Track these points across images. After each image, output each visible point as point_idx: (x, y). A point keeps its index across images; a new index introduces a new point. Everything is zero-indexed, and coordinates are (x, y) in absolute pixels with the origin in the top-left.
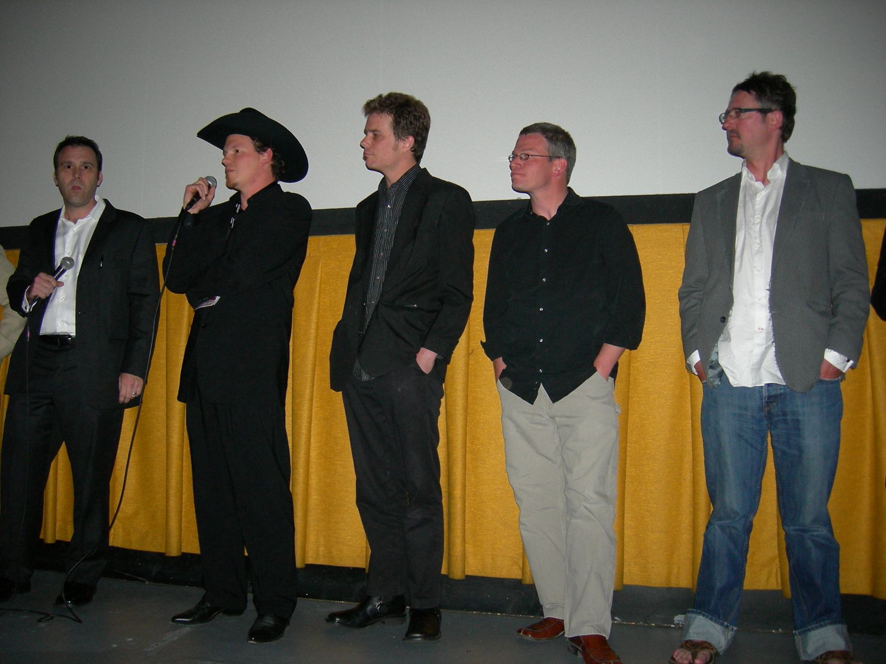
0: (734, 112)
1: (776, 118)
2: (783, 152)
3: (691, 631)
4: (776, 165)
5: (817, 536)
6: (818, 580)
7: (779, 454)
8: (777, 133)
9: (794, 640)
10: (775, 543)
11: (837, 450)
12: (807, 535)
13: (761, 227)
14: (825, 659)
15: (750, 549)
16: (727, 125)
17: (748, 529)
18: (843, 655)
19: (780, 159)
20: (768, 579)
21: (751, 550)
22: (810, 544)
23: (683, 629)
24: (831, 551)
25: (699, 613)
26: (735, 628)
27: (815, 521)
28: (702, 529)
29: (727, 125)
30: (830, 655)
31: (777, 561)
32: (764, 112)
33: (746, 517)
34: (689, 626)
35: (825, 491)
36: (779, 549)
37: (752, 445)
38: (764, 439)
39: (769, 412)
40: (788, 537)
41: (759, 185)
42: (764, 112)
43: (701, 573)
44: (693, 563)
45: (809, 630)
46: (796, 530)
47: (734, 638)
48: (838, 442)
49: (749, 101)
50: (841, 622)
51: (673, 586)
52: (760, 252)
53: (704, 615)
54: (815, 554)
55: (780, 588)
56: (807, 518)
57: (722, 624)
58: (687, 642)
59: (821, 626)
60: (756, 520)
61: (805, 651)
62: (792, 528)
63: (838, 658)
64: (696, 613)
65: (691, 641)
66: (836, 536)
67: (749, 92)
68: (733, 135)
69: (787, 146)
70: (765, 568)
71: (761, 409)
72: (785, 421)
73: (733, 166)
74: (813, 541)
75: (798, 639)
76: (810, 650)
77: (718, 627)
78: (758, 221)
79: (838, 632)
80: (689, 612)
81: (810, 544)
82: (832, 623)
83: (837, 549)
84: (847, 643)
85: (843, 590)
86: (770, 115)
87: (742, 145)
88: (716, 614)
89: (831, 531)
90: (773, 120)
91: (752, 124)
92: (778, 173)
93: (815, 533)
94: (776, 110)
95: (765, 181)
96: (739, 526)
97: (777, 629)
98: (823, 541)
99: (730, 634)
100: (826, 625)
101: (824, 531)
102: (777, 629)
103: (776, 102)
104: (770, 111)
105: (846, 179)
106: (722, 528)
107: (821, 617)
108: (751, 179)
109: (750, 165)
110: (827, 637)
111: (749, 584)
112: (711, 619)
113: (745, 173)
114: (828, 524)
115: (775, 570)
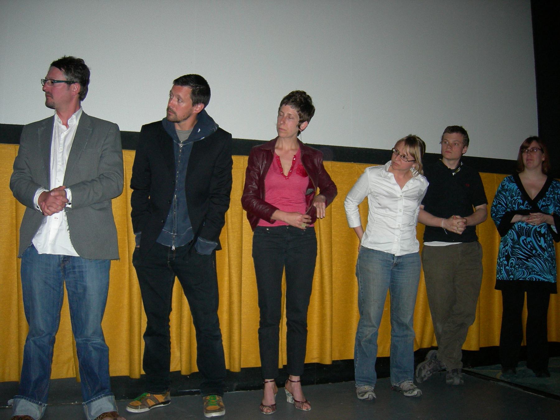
0: (49, 82)
1: (76, 87)
2: (80, 107)
3: (17, 409)
4: (74, 116)
5: (95, 343)
6: (96, 370)
7: (71, 293)
8: (76, 96)
9: (83, 408)
10: (71, 349)
11: (107, 289)
12: (89, 343)
13: (63, 155)
14: (102, 418)
15: (54, 354)
16: (45, 88)
17: (53, 342)
18: (113, 414)
19: (77, 112)
20: (68, 371)
21: (55, 354)
22: (91, 349)
23: (13, 408)
24: (104, 351)
25: (22, 398)
26: (46, 405)
27: (94, 333)
28: (24, 343)
29: (45, 88)
30: (105, 415)
31: (73, 360)
32: (69, 83)
33: (50, 334)
34: (16, 406)
35: (100, 315)
36: (74, 352)
37: (53, 289)
38: (61, 284)
39: (64, 267)
40: (78, 345)
41: (64, 127)
42: (69, 83)
43: (23, 372)
44: (19, 366)
45: (92, 401)
46: (83, 340)
47: (46, 411)
48: (108, 283)
49: (61, 75)
50: (111, 395)
51: (6, 381)
52: (60, 170)
53: (25, 399)
54: (94, 354)
55: (75, 376)
56: (90, 331)
57: (37, 403)
58: (15, 417)
59: (99, 398)
60: (58, 337)
61: (90, 414)
62: (80, 339)
63: (110, 416)
64: (20, 397)
65: (17, 416)
66: (107, 343)
67: (60, 69)
68: (49, 95)
69: (82, 103)
70: (64, 364)
71: (59, 265)
72: (74, 273)
73: (51, 112)
74: (93, 347)
75: (85, 407)
76: (93, 413)
77: (35, 405)
78: (61, 151)
79: (109, 401)
80: (16, 397)
81: (91, 349)
82: (105, 396)
83: (108, 350)
84: (115, 407)
85: (112, 374)
86: (72, 85)
87: (54, 103)
88: (33, 397)
89: (104, 340)
90: (74, 88)
91: (61, 90)
92: (74, 121)
93: (94, 342)
94: (76, 82)
95: (67, 125)
96: (46, 340)
97: (74, 402)
98: (99, 346)
99: (43, 409)
100: (102, 397)
101: (99, 341)
102: (74, 402)
103: (76, 77)
104: (74, 82)
105: (116, 126)
106: (35, 342)
107: (99, 392)
108: (60, 122)
109: (58, 112)
110: (104, 404)
111: (54, 376)
112: (30, 401)
113: (56, 117)
114: (102, 335)
115: (72, 365)
